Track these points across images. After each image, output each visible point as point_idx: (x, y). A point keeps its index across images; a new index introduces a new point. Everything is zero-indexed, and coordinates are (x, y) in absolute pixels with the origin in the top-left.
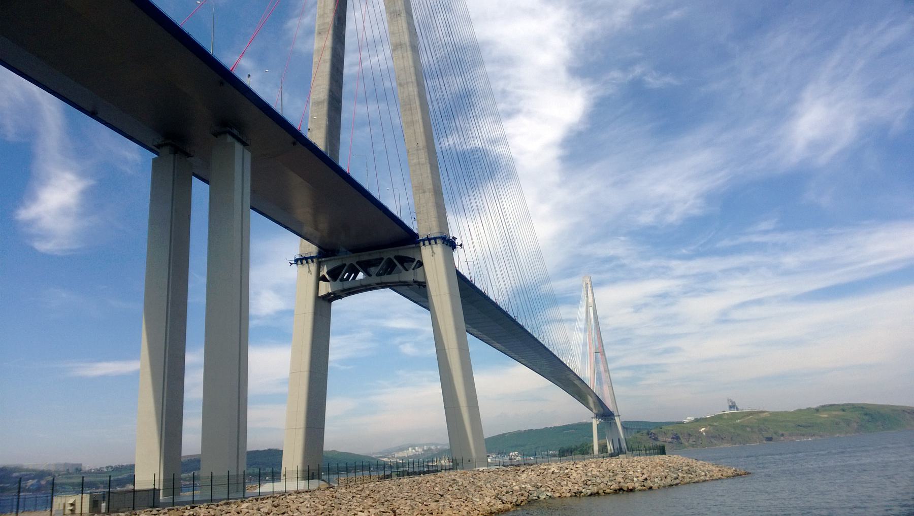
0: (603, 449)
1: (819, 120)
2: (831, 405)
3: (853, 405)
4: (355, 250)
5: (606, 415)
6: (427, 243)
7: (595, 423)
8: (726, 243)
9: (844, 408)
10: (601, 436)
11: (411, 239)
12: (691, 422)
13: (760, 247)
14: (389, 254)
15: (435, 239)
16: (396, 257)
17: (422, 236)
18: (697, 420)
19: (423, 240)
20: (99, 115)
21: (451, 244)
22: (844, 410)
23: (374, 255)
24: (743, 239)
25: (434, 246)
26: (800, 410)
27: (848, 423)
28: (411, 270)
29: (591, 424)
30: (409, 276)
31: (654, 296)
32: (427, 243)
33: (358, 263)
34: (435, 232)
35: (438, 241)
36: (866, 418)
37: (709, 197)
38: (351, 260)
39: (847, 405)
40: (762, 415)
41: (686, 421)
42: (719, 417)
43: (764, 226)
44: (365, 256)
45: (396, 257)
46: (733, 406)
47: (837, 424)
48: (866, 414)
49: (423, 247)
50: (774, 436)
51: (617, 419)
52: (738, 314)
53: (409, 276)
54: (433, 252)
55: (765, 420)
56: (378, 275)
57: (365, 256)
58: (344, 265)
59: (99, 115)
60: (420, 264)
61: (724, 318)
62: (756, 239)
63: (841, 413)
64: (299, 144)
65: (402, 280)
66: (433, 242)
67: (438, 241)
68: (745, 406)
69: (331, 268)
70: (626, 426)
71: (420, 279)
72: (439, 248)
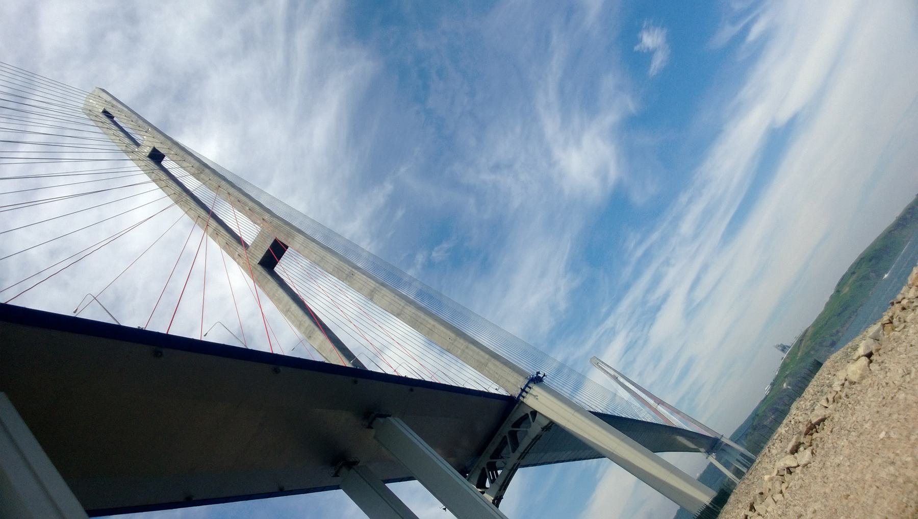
0: (739, 474)
1: (587, 160)
2: (842, 279)
3: (855, 263)
4: (479, 452)
5: (712, 445)
6: (524, 394)
7: (712, 459)
8: (627, 271)
9: (852, 272)
10: (727, 465)
11: (510, 403)
12: (771, 390)
13: (648, 256)
14: (506, 429)
15: (527, 386)
16: (514, 426)
17: (515, 392)
18: (773, 384)
19: (520, 395)
20: (286, 489)
21: (537, 380)
22: (854, 273)
23: (497, 440)
24: (633, 260)
25: (531, 391)
26: (827, 304)
27: (866, 278)
28: (533, 424)
29: (711, 464)
30: (535, 429)
31: (626, 352)
32: (524, 394)
33: (492, 457)
34: (522, 382)
35: (530, 385)
36: (873, 262)
37: (573, 267)
38: (484, 461)
39: (852, 266)
40: (809, 334)
41: (767, 392)
42: (784, 367)
43: (631, 244)
44: (491, 449)
45: (514, 426)
46: (783, 348)
47: (861, 286)
48: (870, 260)
49: (525, 400)
50: (834, 338)
51: (723, 440)
52: (700, 294)
53: (535, 429)
54: (535, 396)
55: (815, 334)
56: (514, 451)
57: (491, 449)
58: (484, 469)
59: (286, 489)
60: (534, 413)
61: (691, 311)
62: (640, 252)
63: (855, 277)
64: (414, 388)
65: (534, 436)
66: (527, 389)
67: (530, 385)
68: (790, 340)
69: (476, 482)
70: (736, 438)
71: (545, 423)
72: (536, 390)
